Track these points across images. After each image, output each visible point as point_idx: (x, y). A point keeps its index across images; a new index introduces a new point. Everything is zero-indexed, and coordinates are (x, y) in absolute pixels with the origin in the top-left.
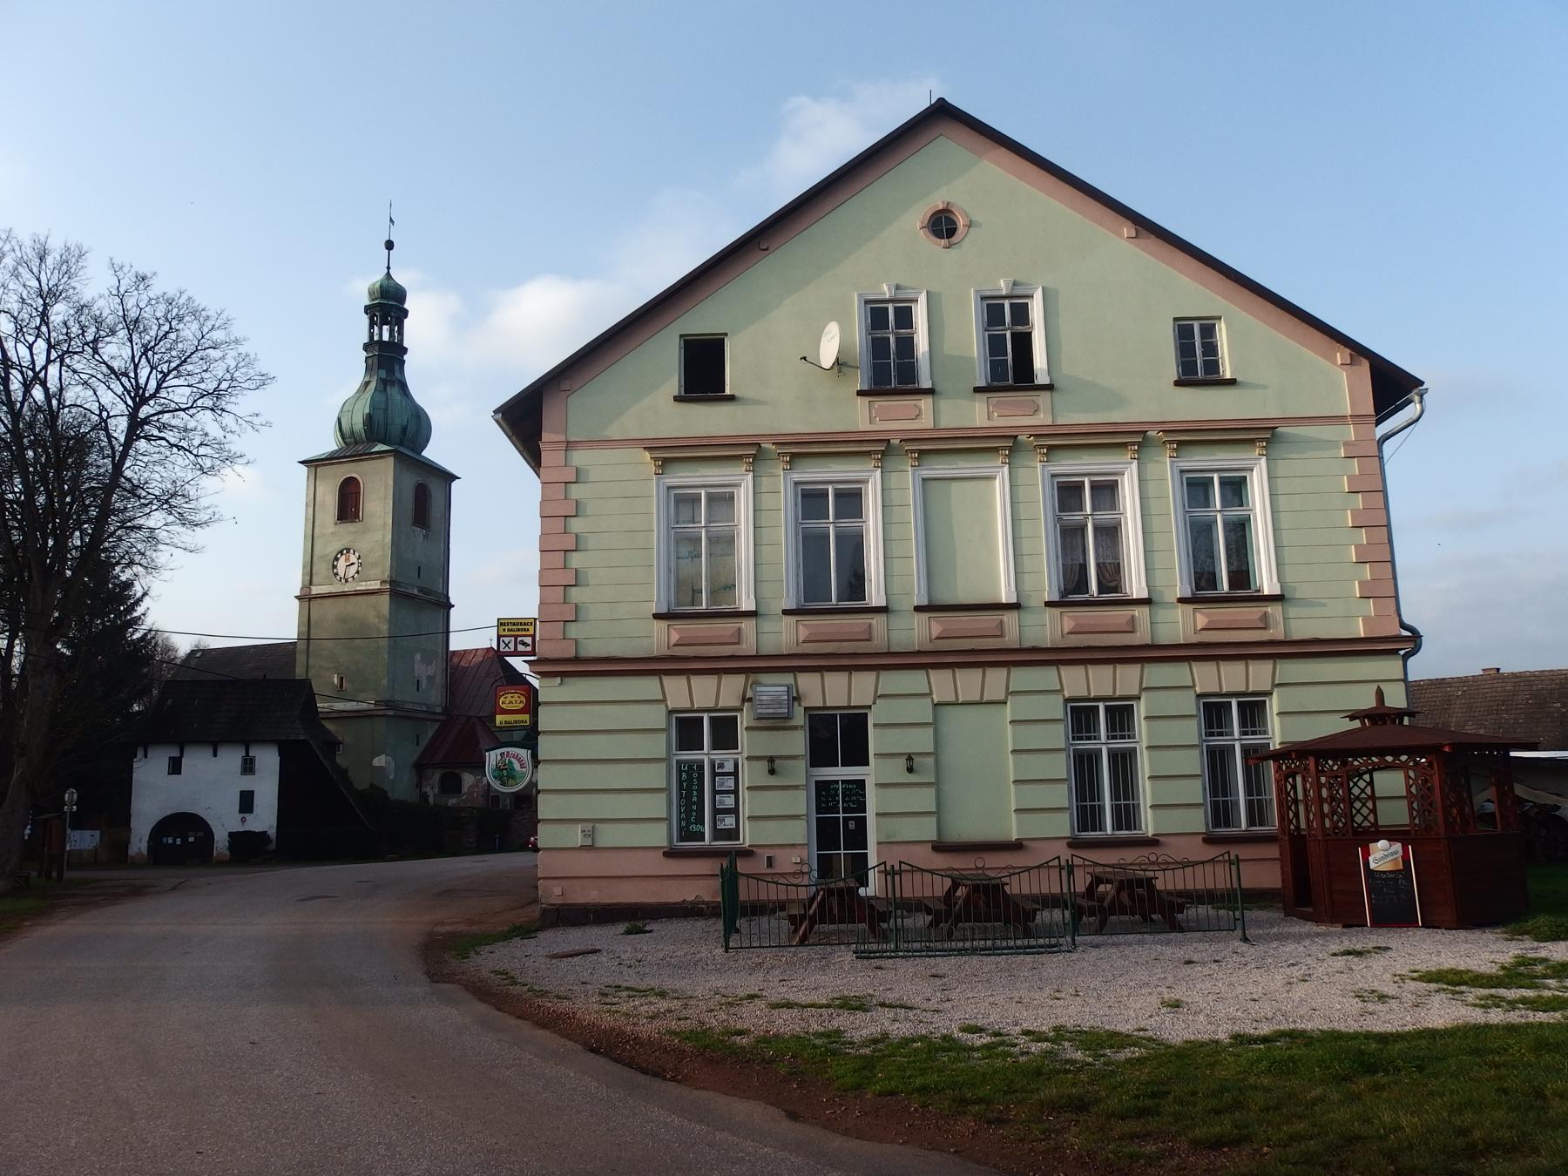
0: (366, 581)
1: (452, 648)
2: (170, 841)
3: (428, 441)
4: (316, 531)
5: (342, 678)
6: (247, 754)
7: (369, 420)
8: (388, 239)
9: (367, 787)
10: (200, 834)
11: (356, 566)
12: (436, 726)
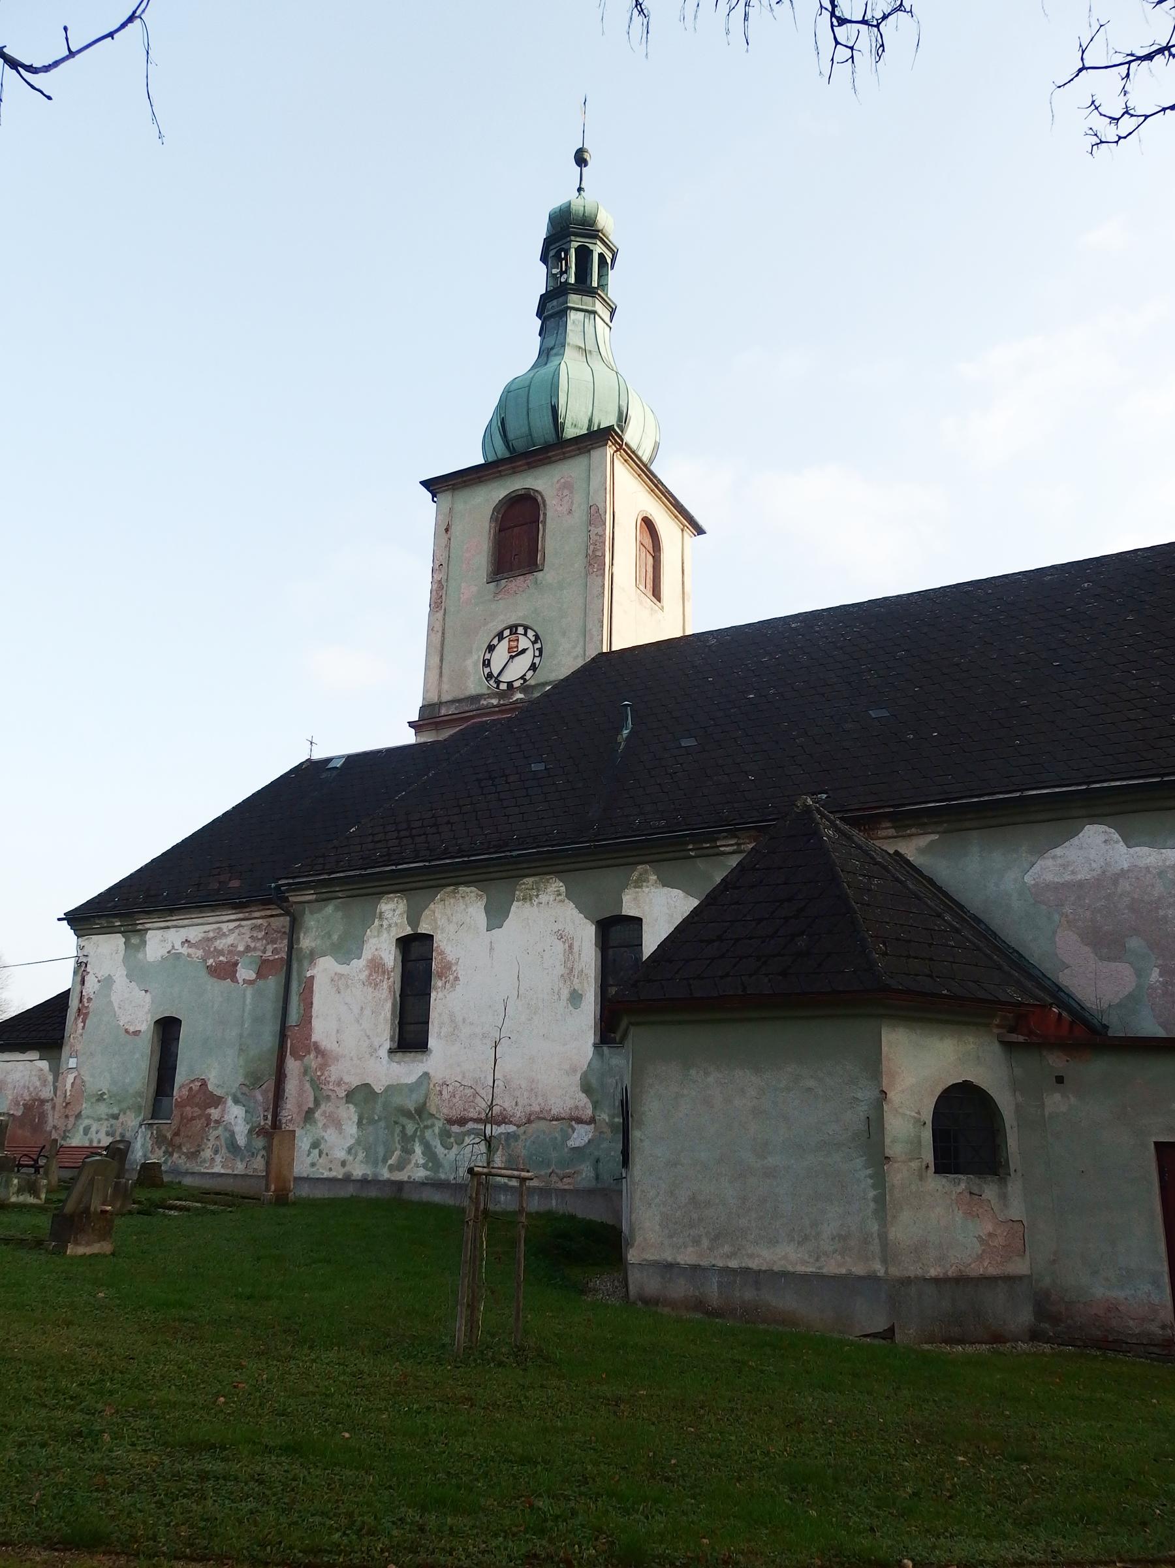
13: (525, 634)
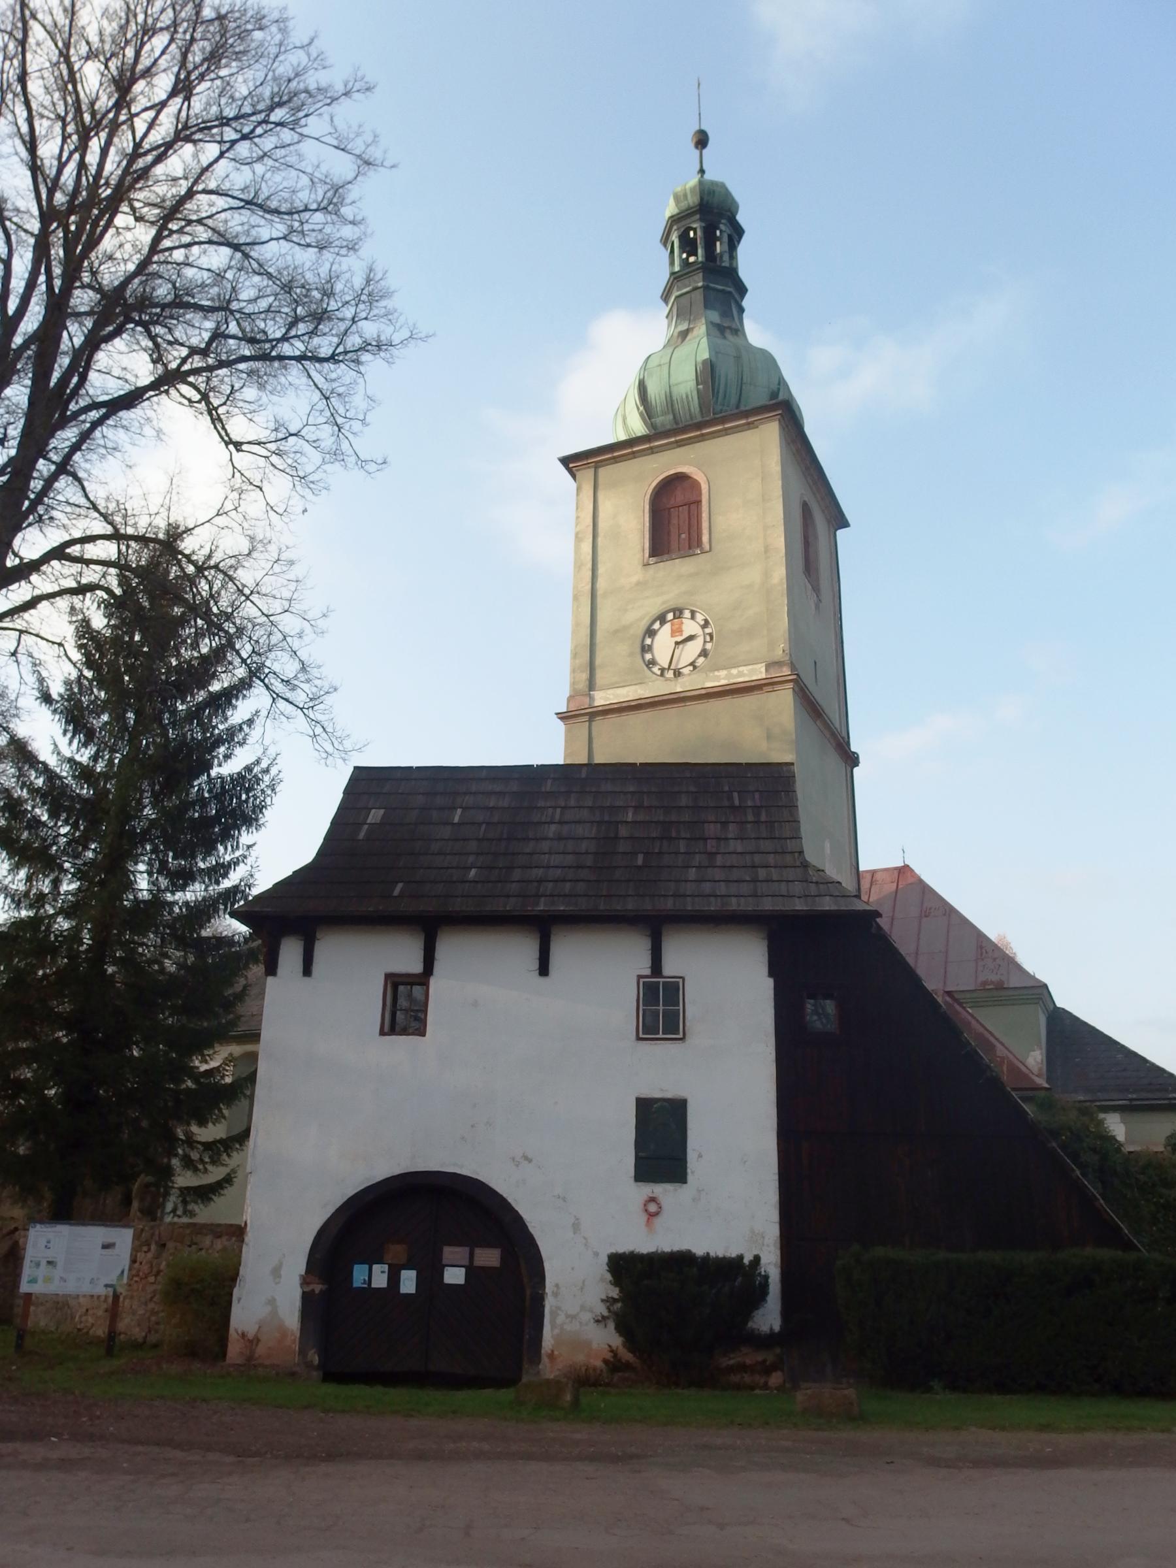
0: (725, 668)
2: (380, 1279)
4: (601, 584)
6: (657, 966)
8: (697, 128)
10: (489, 1257)
13: (693, 617)
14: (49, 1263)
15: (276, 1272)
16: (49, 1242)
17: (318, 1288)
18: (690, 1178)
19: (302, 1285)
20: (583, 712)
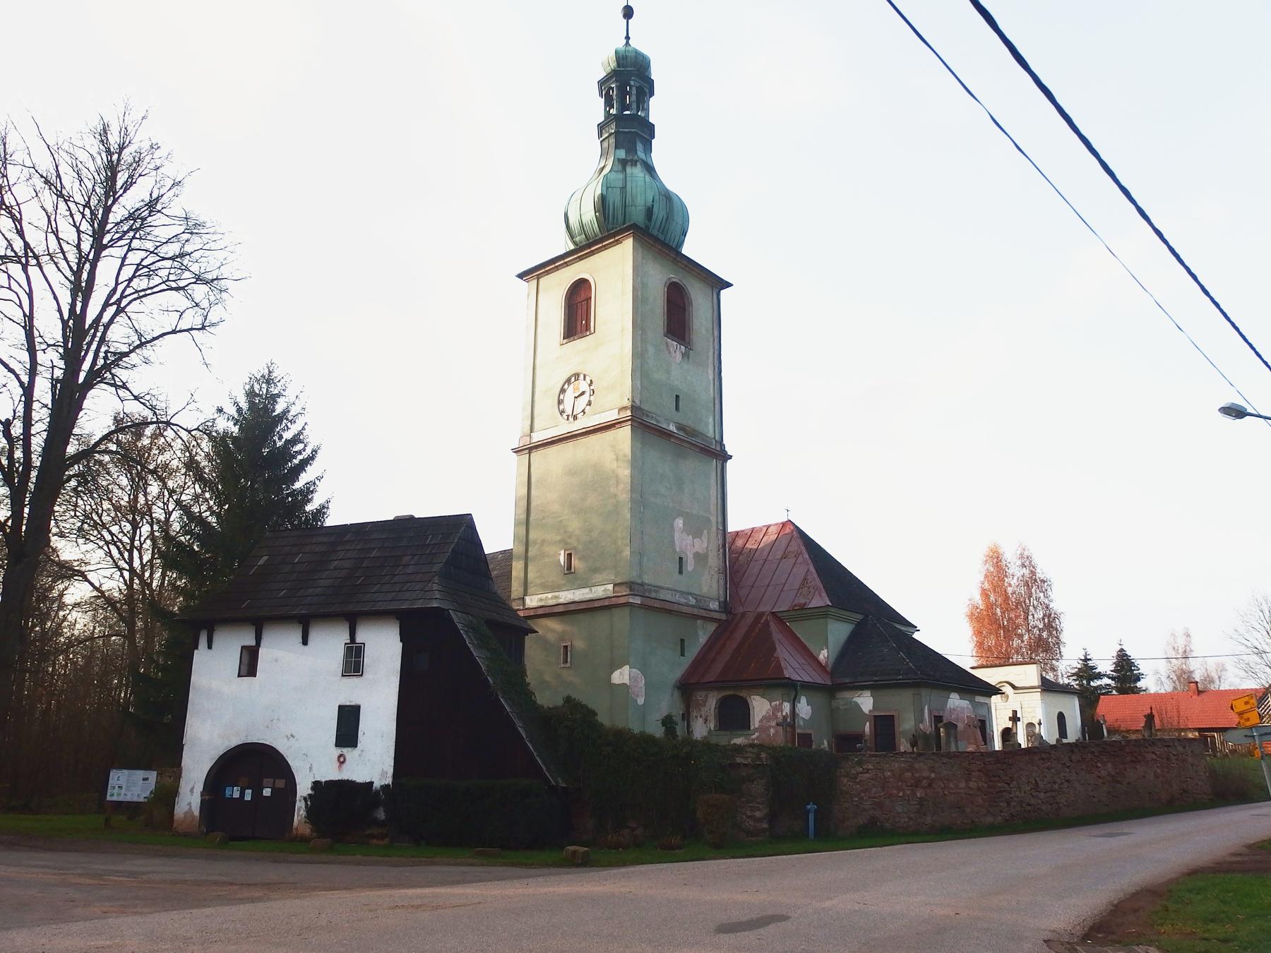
1: (732, 527)
2: (236, 795)
3: (684, 233)
5: (570, 555)
7: (603, 205)
9: (560, 702)
10: (281, 784)
11: (587, 395)
12: (712, 627)
14: (119, 787)
15: (192, 790)
16: (119, 777)
17: (207, 798)
18: (359, 745)
19: (202, 796)
20: (524, 447)
